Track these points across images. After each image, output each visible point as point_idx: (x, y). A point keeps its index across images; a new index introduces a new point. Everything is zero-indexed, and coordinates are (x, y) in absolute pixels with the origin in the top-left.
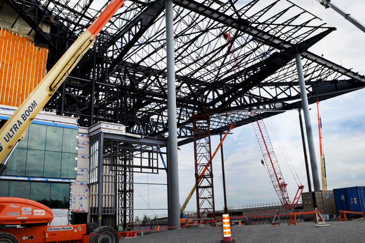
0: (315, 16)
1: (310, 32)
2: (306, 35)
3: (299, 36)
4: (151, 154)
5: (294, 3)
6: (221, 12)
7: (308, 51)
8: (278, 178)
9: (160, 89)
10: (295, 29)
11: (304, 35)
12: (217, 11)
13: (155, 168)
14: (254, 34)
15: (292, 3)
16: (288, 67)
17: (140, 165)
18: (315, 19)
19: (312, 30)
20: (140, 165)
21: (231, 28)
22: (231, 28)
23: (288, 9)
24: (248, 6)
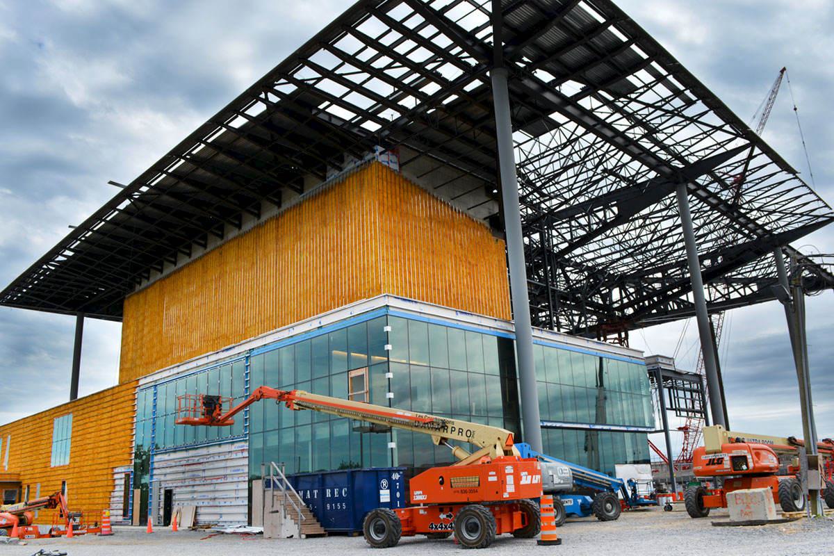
0: (803, 183)
1: (766, 189)
2: (694, 141)
3: (779, 225)
4: (672, 390)
5: (820, 196)
6: (713, 191)
7: (431, 7)
8: (453, 506)
9: (575, 269)
10: (662, 118)
11: (663, 121)
12: (715, 195)
13: (683, 410)
14: (589, 125)
15: (810, 189)
16: (546, 163)
17: (86, 319)
18: (793, 180)
19: (810, 219)
20: (86, 319)
21: (468, 55)
22: (468, 55)
23: (792, 189)
24: (758, 192)
